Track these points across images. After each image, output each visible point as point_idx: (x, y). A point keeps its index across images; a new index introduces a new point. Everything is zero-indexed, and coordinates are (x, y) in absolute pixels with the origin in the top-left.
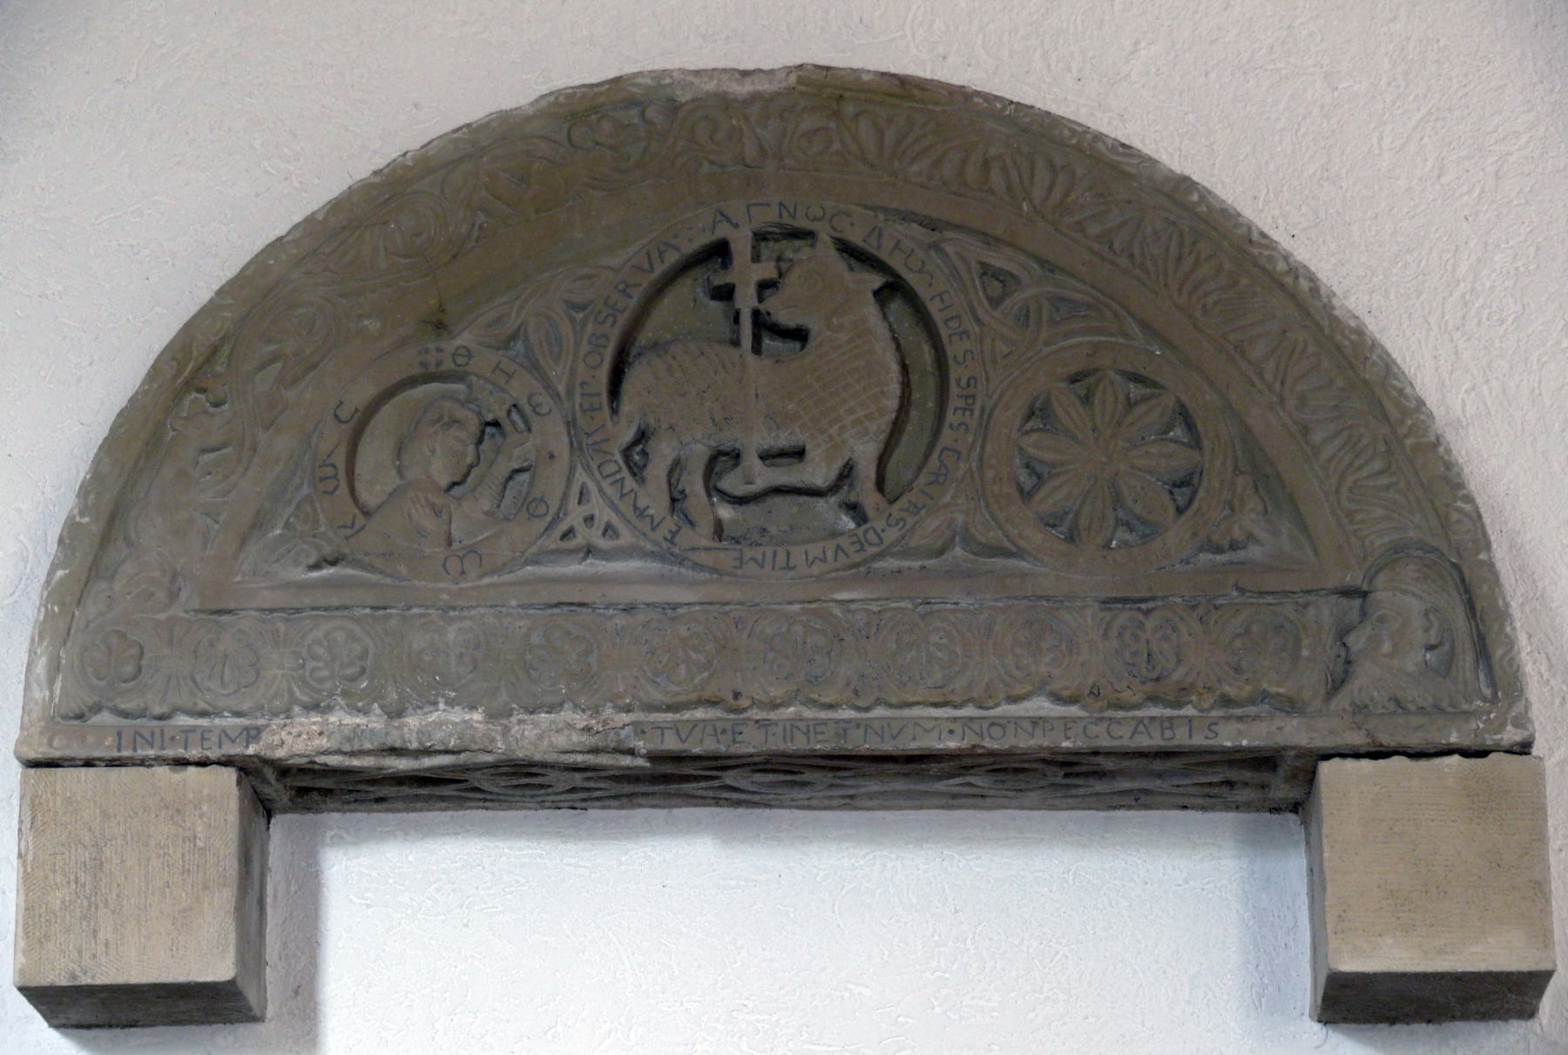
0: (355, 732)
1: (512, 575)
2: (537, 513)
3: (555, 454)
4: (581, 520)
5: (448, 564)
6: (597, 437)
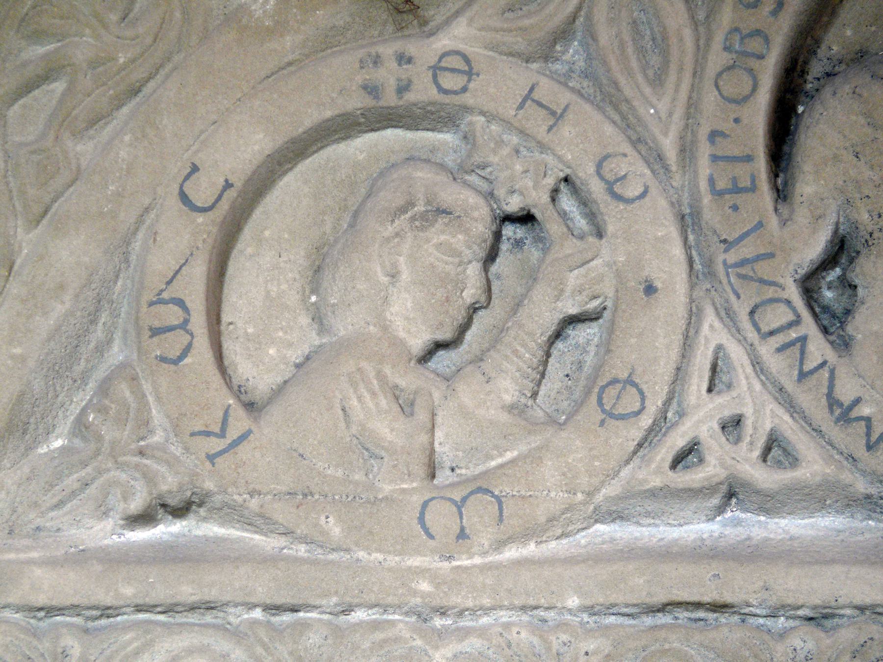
1: (564, 541)
2: (620, 410)
3: (658, 284)
4: (716, 427)
5: (428, 517)
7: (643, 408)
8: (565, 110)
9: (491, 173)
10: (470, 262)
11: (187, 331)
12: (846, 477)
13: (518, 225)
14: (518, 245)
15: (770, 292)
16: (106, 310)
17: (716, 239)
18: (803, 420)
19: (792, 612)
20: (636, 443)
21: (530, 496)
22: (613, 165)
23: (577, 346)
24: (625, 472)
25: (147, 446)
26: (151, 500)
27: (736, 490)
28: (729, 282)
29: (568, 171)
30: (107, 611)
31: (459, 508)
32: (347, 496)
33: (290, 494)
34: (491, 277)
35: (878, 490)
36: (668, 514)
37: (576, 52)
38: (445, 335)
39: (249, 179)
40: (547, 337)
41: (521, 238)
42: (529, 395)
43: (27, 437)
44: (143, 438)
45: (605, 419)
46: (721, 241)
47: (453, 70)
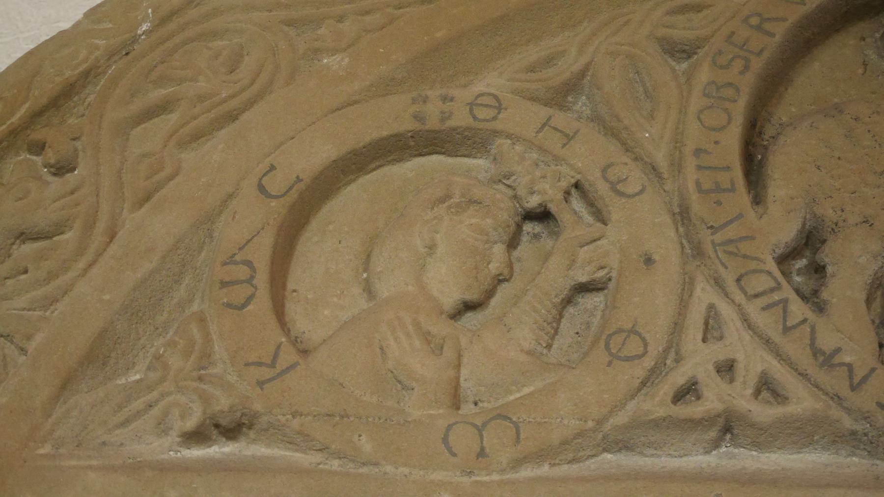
1: (575, 466)
2: (624, 353)
3: (656, 257)
4: (711, 367)
5: (452, 438)
6: (731, 232)
7: (645, 352)
8: (576, 133)
9: (515, 181)
10: (496, 243)
11: (252, 285)
12: (836, 412)
13: (536, 223)
14: (536, 237)
15: (753, 265)
16: (190, 274)
17: (704, 226)
18: (789, 366)
20: (640, 380)
21: (545, 422)
22: (616, 171)
23: (586, 310)
24: (631, 406)
25: (206, 374)
26: (205, 420)
27: (732, 424)
29: (578, 177)
32: (380, 419)
33: (328, 415)
34: (513, 260)
35: (862, 427)
36: (670, 445)
37: (584, 104)
38: (472, 296)
39: (316, 178)
40: (561, 299)
42: (544, 345)
43: (107, 369)
44: (204, 368)
45: (612, 360)
46: (708, 228)
47: (487, 106)
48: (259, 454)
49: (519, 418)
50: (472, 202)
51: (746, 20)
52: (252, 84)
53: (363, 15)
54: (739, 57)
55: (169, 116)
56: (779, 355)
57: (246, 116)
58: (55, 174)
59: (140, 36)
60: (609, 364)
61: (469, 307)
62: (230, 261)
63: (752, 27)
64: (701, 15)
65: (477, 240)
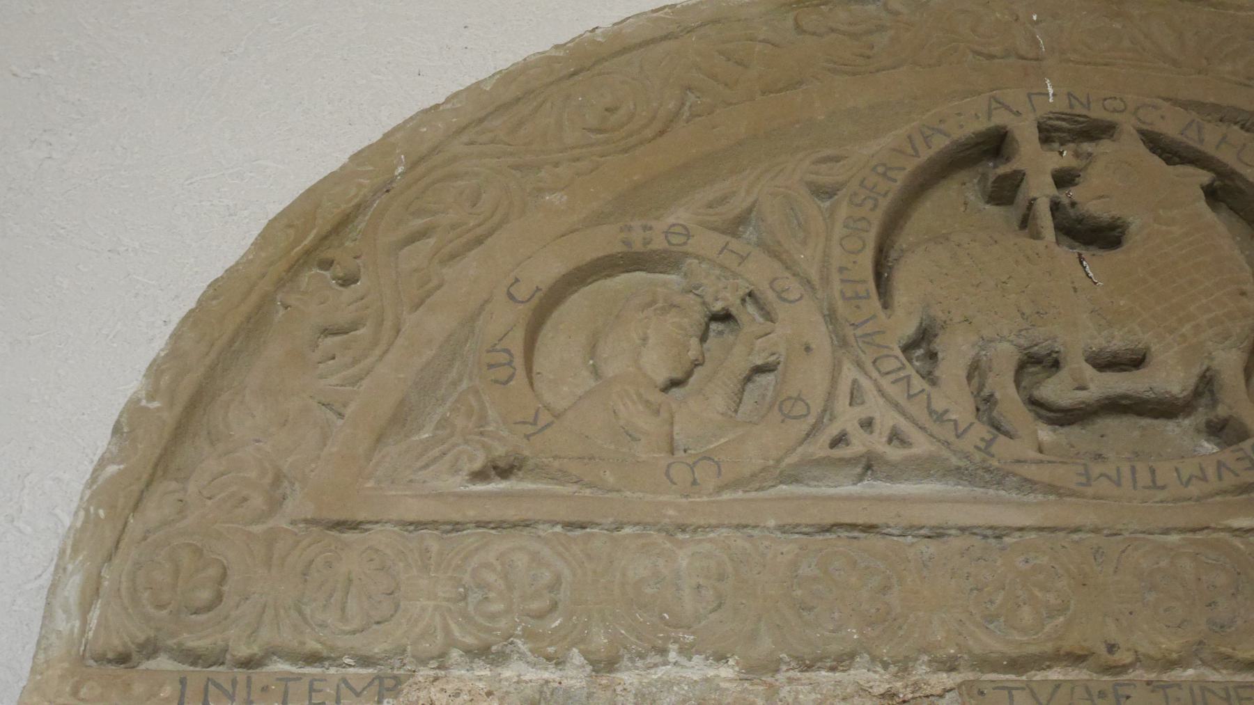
0: (541, 692)
2: (794, 413)
3: (813, 346)
6: (868, 328)
8: (749, 254)
10: (691, 337)
11: (511, 367)
12: (945, 453)
15: (885, 352)
19: (916, 532)
20: (806, 432)
24: (800, 450)
28: (858, 346)
30: (457, 526)
31: (692, 469)
37: (751, 233)
38: (678, 375)
41: (722, 330)
44: (482, 426)
48: (526, 488)
49: (719, 459)
50: (673, 306)
51: (874, 169)
52: (492, 217)
53: (574, 161)
54: (869, 197)
55: (427, 240)
56: (903, 413)
57: (489, 241)
58: (342, 285)
59: (397, 176)
60: (783, 421)
61: (675, 383)
62: (492, 350)
63: (879, 174)
64: (839, 164)
65: (679, 334)
